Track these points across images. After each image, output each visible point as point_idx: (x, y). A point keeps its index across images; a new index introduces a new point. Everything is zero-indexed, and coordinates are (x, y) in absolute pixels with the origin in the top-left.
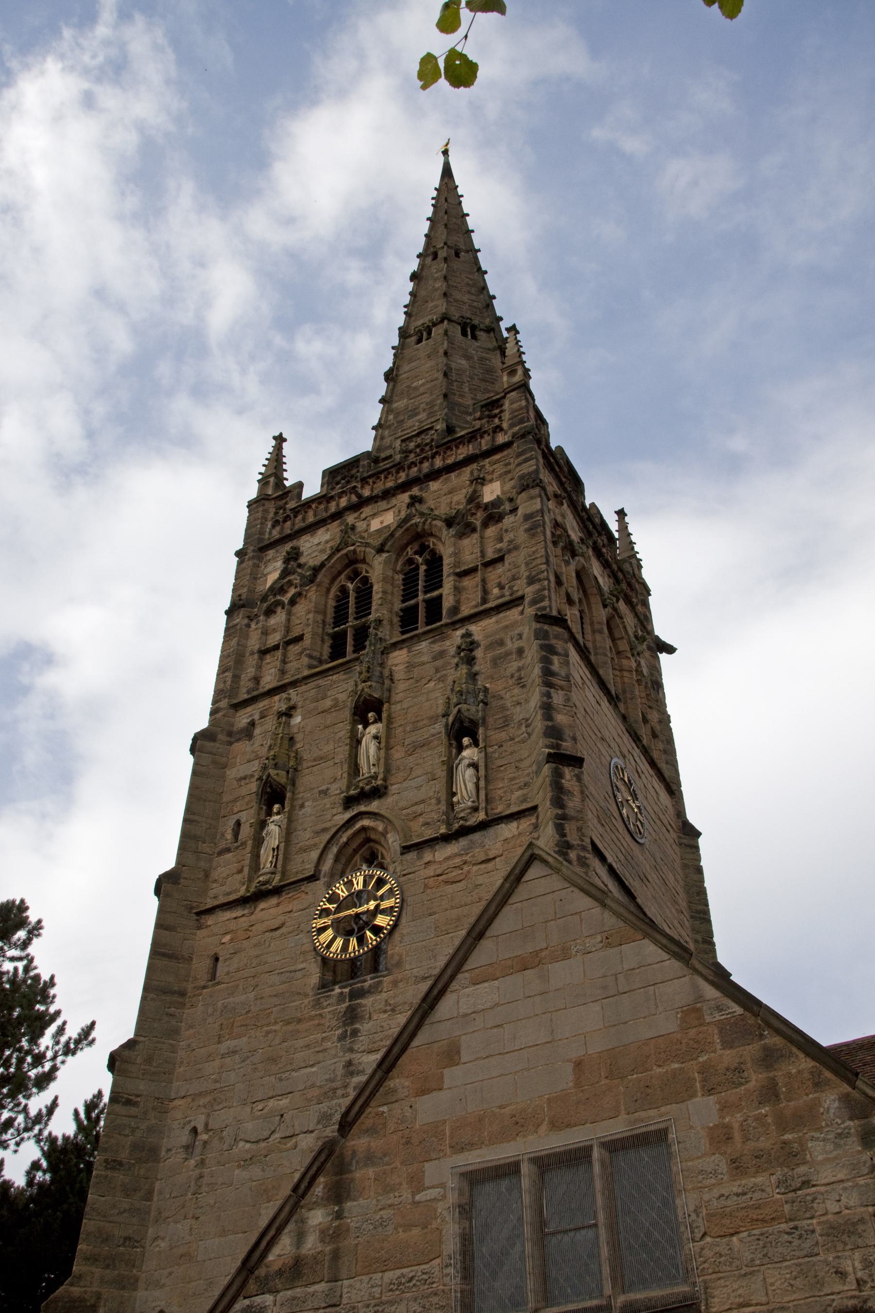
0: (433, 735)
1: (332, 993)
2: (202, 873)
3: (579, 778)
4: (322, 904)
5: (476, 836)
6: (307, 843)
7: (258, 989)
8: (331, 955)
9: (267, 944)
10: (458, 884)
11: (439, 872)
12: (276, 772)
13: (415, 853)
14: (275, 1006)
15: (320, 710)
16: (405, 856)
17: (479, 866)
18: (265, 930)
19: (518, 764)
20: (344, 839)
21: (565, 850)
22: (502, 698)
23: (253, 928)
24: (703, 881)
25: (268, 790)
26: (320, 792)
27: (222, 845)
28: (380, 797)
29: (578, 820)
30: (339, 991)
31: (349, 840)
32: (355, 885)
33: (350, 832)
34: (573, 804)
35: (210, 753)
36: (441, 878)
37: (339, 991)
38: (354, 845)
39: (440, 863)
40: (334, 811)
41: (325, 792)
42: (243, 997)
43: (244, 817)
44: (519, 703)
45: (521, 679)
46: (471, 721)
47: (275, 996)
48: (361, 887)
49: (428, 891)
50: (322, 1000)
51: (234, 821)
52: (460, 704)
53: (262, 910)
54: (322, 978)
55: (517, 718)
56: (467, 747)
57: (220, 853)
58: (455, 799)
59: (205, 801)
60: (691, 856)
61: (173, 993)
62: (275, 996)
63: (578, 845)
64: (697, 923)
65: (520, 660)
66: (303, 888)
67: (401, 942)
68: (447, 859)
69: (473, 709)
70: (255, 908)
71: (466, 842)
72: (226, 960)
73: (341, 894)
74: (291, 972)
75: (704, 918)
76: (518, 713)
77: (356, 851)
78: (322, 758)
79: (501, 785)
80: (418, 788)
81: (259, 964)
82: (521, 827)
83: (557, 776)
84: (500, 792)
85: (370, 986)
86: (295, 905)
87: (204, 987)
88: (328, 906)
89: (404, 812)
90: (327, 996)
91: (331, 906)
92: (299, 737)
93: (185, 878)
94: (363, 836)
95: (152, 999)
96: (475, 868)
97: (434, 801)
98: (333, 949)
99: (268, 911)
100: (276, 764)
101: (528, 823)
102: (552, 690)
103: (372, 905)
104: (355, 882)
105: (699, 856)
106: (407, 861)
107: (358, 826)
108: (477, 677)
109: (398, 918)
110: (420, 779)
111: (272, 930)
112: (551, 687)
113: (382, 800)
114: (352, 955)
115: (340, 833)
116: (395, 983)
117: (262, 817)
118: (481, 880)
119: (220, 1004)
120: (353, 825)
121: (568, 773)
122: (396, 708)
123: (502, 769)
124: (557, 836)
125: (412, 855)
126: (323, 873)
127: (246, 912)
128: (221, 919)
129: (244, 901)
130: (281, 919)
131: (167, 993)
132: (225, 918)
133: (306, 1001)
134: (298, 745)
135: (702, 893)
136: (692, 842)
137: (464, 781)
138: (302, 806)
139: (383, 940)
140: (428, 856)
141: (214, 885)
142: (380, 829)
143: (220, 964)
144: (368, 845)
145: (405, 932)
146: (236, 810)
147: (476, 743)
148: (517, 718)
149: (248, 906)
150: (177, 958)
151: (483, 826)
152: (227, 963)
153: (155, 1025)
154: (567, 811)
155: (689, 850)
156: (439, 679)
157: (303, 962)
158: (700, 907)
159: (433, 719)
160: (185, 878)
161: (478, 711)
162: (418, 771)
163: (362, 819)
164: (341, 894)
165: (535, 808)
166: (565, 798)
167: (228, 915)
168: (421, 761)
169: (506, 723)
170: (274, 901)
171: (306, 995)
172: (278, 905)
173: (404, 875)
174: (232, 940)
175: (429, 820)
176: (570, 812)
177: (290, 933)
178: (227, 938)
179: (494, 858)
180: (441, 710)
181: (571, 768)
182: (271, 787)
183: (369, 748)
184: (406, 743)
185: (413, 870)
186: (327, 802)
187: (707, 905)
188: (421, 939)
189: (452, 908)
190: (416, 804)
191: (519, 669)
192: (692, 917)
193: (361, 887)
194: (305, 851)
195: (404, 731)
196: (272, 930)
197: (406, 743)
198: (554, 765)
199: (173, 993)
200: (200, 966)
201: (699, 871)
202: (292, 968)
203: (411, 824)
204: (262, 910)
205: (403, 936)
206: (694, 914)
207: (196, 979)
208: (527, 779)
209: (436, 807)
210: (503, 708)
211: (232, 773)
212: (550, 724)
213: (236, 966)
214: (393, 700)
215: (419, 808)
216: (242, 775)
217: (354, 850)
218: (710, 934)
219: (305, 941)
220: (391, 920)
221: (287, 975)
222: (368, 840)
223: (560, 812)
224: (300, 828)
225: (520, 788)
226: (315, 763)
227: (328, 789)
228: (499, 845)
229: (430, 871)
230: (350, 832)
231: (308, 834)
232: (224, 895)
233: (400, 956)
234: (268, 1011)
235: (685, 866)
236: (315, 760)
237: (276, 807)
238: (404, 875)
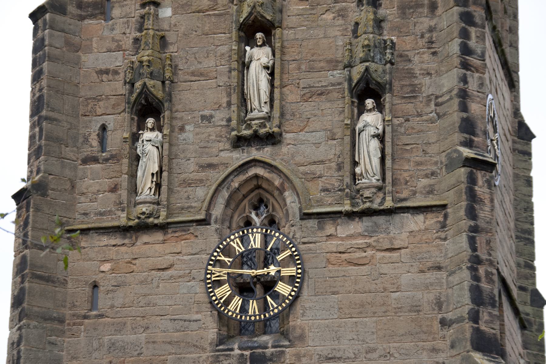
0: (333, 85)
1: (232, 353)
2: (68, 183)
3: (490, 184)
4: (215, 254)
5: (381, 220)
6: (191, 176)
7: (149, 331)
8: (230, 314)
9: (155, 284)
10: (362, 267)
11: (342, 249)
12: (152, 82)
13: (316, 221)
14: (170, 354)
15: (194, 8)
16: (305, 221)
17: (383, 254)
18: (151, 267)
19: (425, 148)
20: (236, 185)
21: (475, 266)
22: (410, 61)
23: (136, 261)
24: (531, 196)
25: (143, 102)
26: (203, 117)
27: (87, 151)
28: (274, 144)
29: (487, 232)
30: (239, 352)
31: (241, 185)
32: (252, 242)
33: (242, 178)
34: (484, 213)
35: (63, 31)
36: (343, 256)
37: (239, 352)
38: (244, 191)
39: (342, 239)
40: (221, 146)
41: (207, 119)
42: (133, 337)
43: (111, 121)
44: (429, 74)
45: (432, 43)
46: (378, 84)
47: (170, 343)
48: (258, 245)
49: (331, 267)
50: (221, 358)
51: (99, 126)
52: (368, 61)
53: (146, 243)
54: (219, 334)
55: (427, 91)
56: (370, 111)
57: (85, 161)
58: (358, 170)
59: (63, 94)
60: (523, 165)
61: (51, 319)
62: (170, 343)
63: (487, 260)
64: (521, 244)
65: (432, 18)
66: (192, 230)
67: (303, 315)
68: (351, 237)
69: (380, 68)
70: (137, 239)
71: (370, 224)
72: (108, 292)
73: (237, 248)
74: (185, 320)
75: (528, 239)
76: (427, 86)
77: (245, 197)
78: (202, 75)
79: (407, 167)
80: (317, 145)
81: (148, 305)
82: (427, 223)
83: (472, 180)
84: (406, 174)
85: (272, 354)
86: (181, 246)
87: (85, 317)
88: (223, 258)
89: (302, 169)
90: (227, 355)
91: (226, 259)
92: (171, 37)
93: (53, 190)
94: (254, 182)
95: (35, 327)
96: (380, 255)
97: (334, 165)
98: (231, 307)
99: (151, 246)
100: (151, 73)
101: (435, 220)
102: (469, 73)
103: (272, 270)
104: (252, 239)
105: (530, 165)
106: (307, 227)
108: (383, 24)
109: (300, 289)
110: (318, 134)
111: (159, 269)
112: (467, 69)
113: (276, 148)
114: (253, 318)
115: (232, 177)
117: (135, 130)
118: (385, 269)
119: (106, 339)
120: (246, 170)
121: (481, 176)
122: (288, 34)
123: (408, 148)
124: (470, 250)
125: (312, 223)
126: (213, 218)
127: (126, 241)
128: (98, 243)
129: (124, 230)
130: (170, 258)
131: (48, 319)
132: (102, 244)
133: (204, 356)
134: (172, 48)
135: (529, 208)
136: (525, 148)
137: (368, 152)
138: (182, 129)
139: (284, 309)
140: (330, 229)
141: (83, 199)
142: (277, 183)
143: (101, 295)
144: (257, 192)
145: (307, 305)
146: (99, 111)
147: (379, 107)
148: (427, 91)
149: (128, 235)
150: (53, 282)
151: (390, 212)
152: (110, 295)
153: (40, 355)
154: (478, 223)
155: (521, 157)
156: (339, 11)
157: (197, 313)
158: (527, 226)
159: (333, 64)
160: (53, 190)
161: (384, 71)
162: (315, 124)
163: (255, 165)
164: (237, 248)
165: (444, 206)
166: (477, 207)
167: (105, 240)
168: (319, 113)
169: (413, 93)
170: (159, 236)
171: (204, 349)
172: (164, 242)
173: (304, 243)
174: (113, 270)
175: (329, 187)
176: (481, 223)
177: (180, 277)
178: (106, 267)
179: (399, 249)
180: (340, 54)
181: (483, 172)
182: (146, 99)
183: (258, 80)
184: (302, 86)
185: (314, 239)
186: (212, 131)
187: (532, 224)
188: (324, 317)
189: (356, 292)
190: (315, 163)
191: (431, 30)
192: (517, 237)
193: (258, 245)
194: (189, 185)
195: (299, 68)
196: (159, 269)
197: (302, 86)
198: (469, 169)
199: (51, 319)
200: (77, 291)
201: (529, 182)
202: (187, 317)
203: (309, 184)
204: (146, 243)
205: (304, 309)
206: (519, 234)
207: (74, 306)
208: (434, 168)
209: (336, 174)
210: (411, 74)
211: (92, 61)
212: (465, 115)
213: (121, 301)
214: (285, 24)
215: (318, 169)
216: (103, 67)
217: (244, 195)
218: (532, 256)
219: (198, 290)
220: (293, 291)
221: (181, 323)
222: (258, 187)
223: (472, 223)
224: (182, 156)
225: (426, 176)
226: (194, 78)
227: (212, 116)
228: (404, 235)
229: (332, 245)
230: (242, 178)
231: (192, 166)
232: (96, 214)
233: (303, 330)
234: (162, 358)
235: (516, 177)
236: (193, 74)
237: (150, 122)
238: (304, 243)
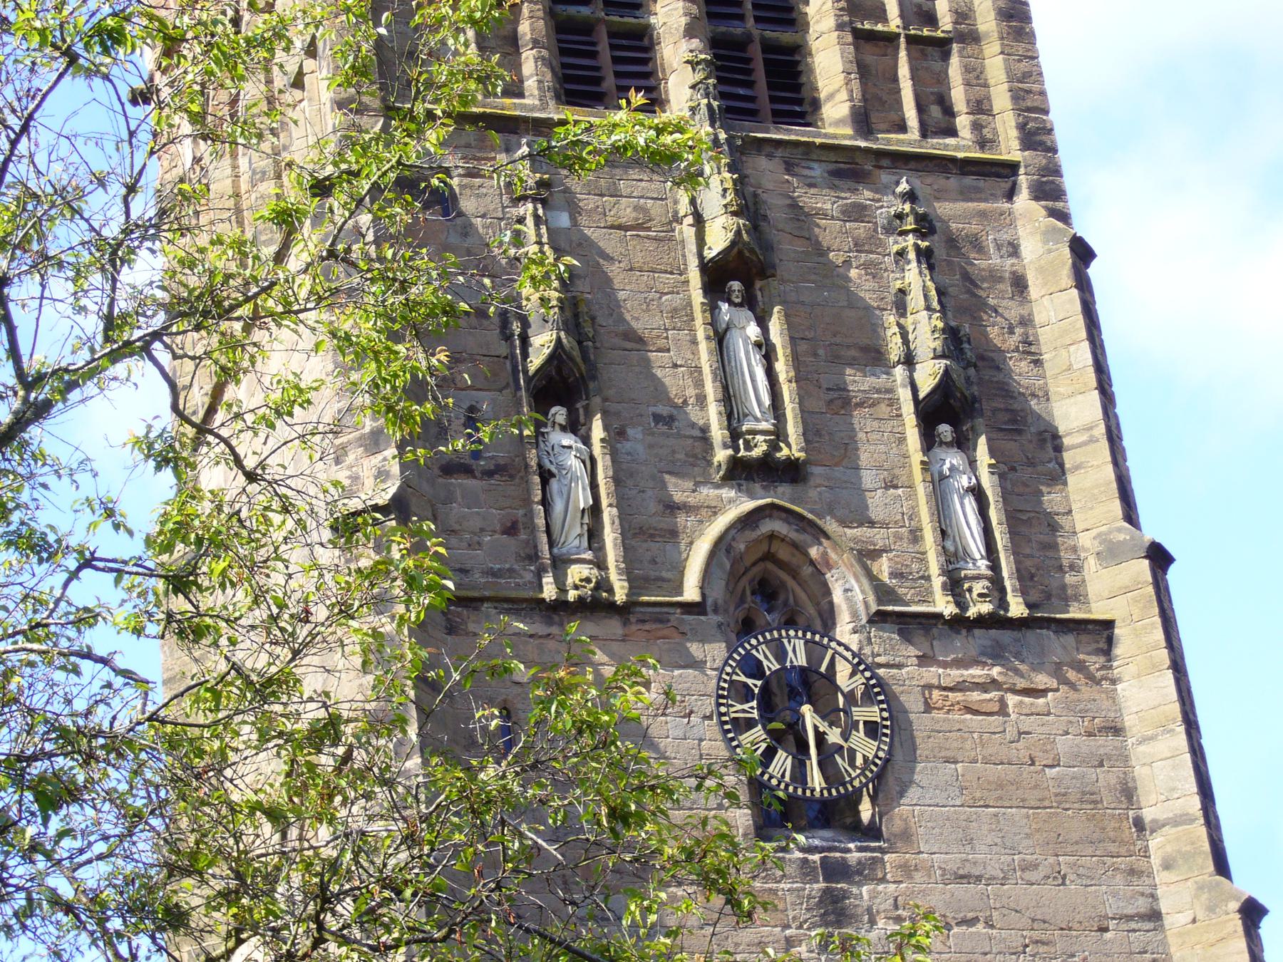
107: (768, 526)
116: (907, 870)
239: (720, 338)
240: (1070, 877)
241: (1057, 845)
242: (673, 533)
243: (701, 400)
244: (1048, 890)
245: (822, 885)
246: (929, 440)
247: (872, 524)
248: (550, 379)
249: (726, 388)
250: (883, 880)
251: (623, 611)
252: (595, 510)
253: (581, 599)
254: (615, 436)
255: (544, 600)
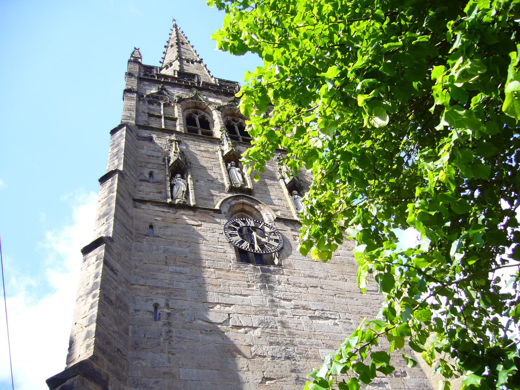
239: (228, 171)
240: (348, 280)
241: (343, 272)
242: (212, 200)
243: (222, 179)
244: (341, 282)
245: (261, 273)
246: (291, 193)
247: (275, 205)
248: (175, 166)
249: (230, 179)
250: (283, 274)
251: (194, 209)
252: (187, 192)
253: (179, 204)
254: (195, 181)
255: (374, 360)
